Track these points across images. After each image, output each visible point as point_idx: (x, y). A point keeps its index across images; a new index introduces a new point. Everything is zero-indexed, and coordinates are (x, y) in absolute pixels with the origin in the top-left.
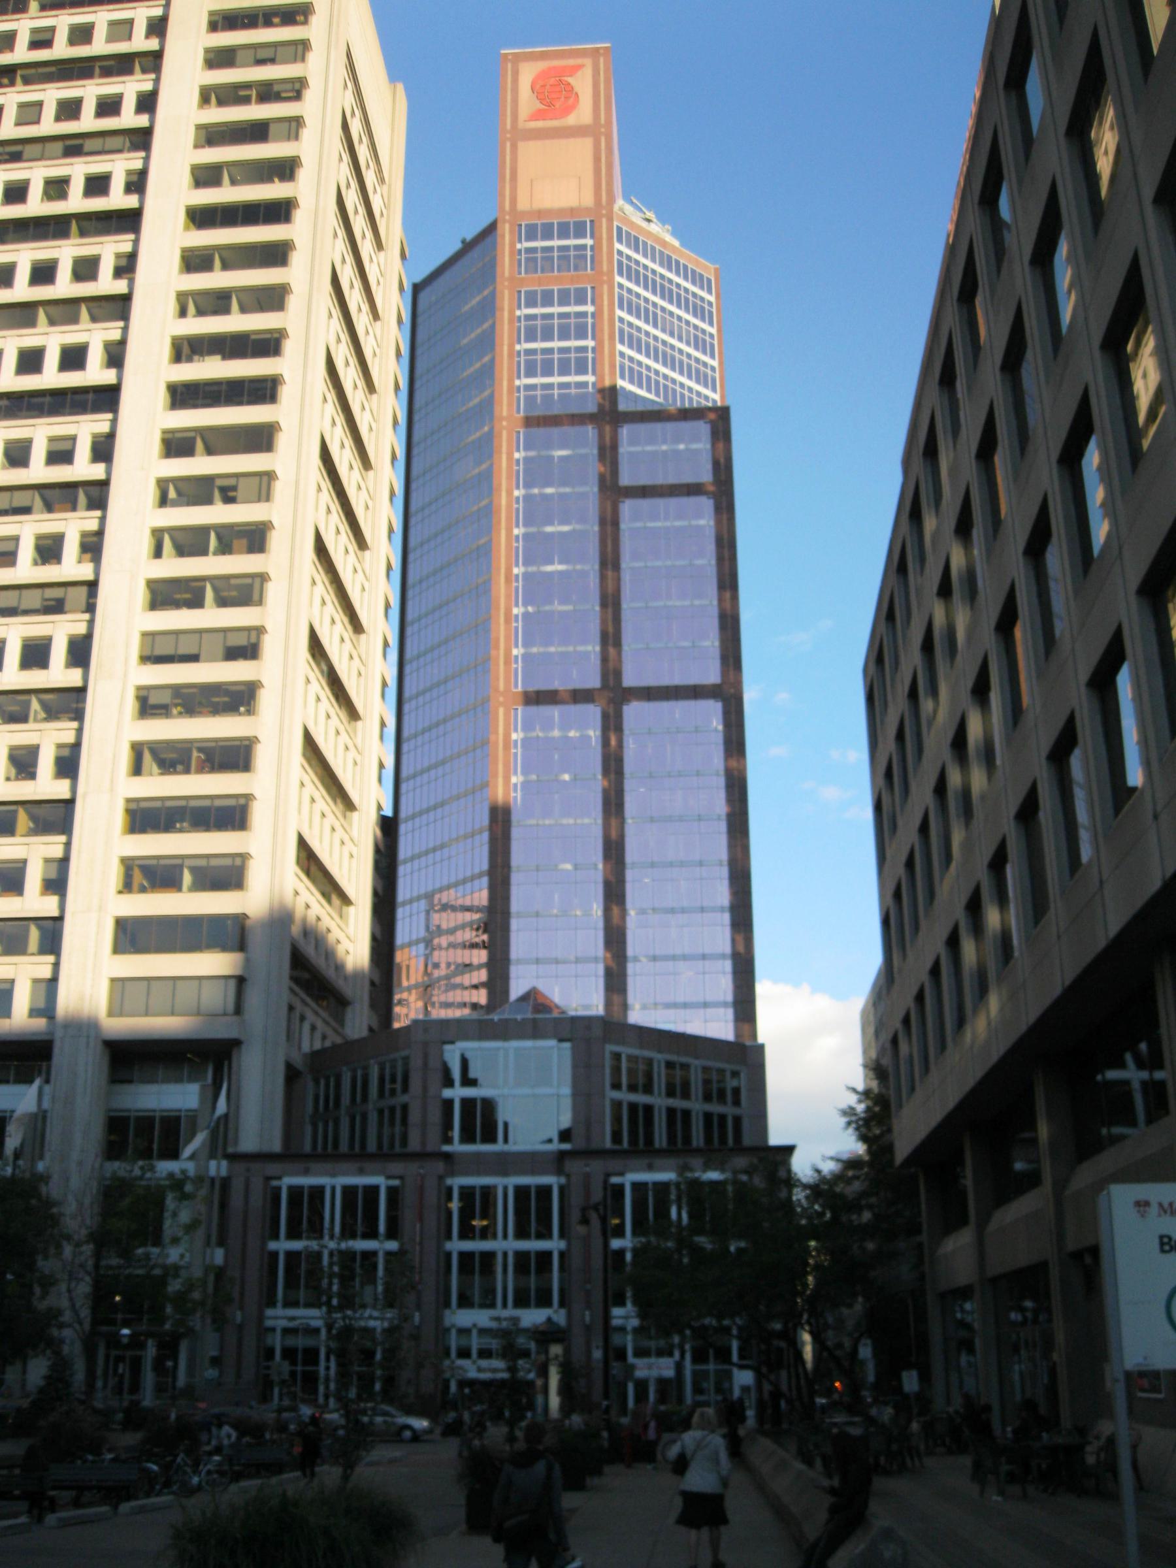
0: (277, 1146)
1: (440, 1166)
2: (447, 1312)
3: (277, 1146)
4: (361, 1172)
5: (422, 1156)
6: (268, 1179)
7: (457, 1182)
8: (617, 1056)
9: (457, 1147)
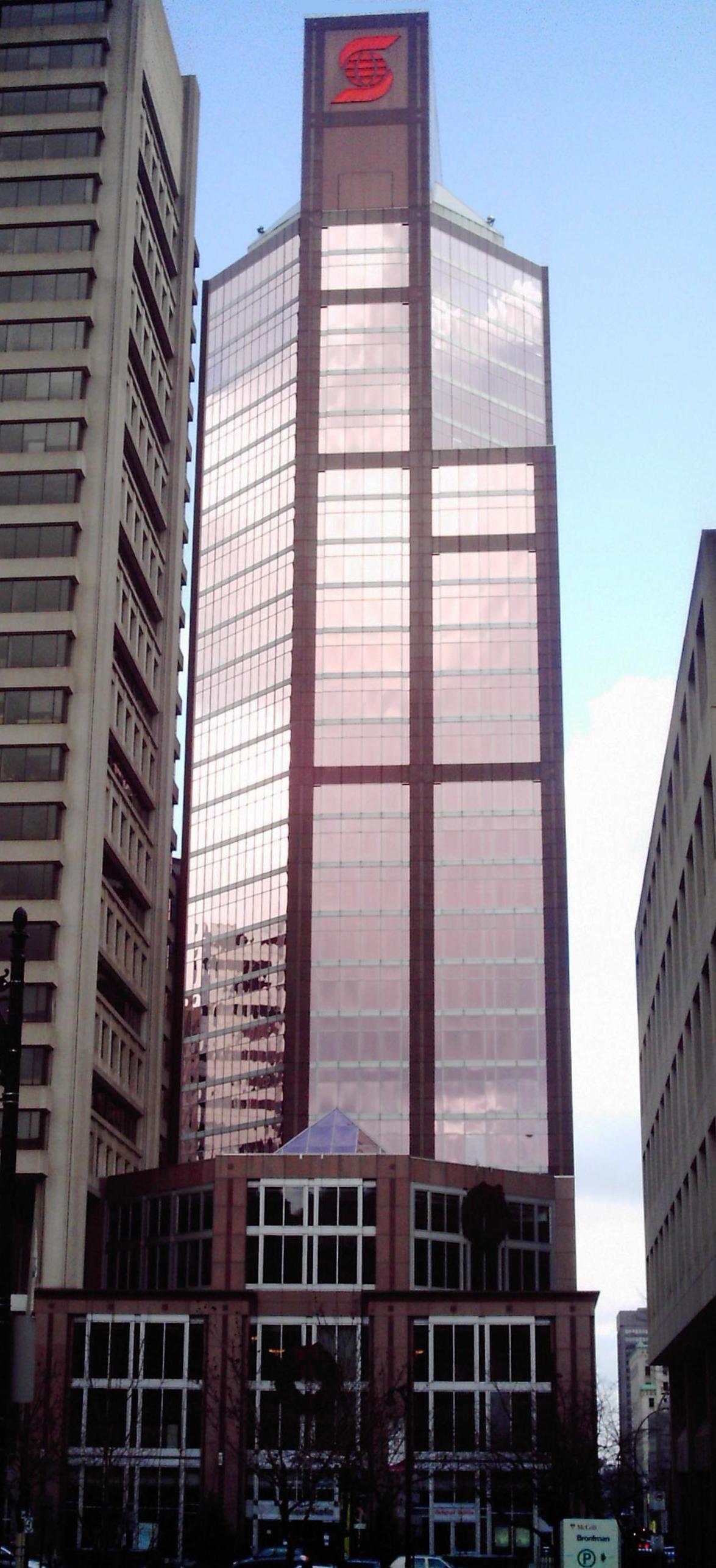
0: (78, 1283)
1: (245, 1306)
2: (249, 1502)
3: (78, 1283)
4: (165, 1310)
5: (229, 1295)
6: (71, 1316)
7: (263, 1321)
8: (421, 1195)
9: (261, 1286)
